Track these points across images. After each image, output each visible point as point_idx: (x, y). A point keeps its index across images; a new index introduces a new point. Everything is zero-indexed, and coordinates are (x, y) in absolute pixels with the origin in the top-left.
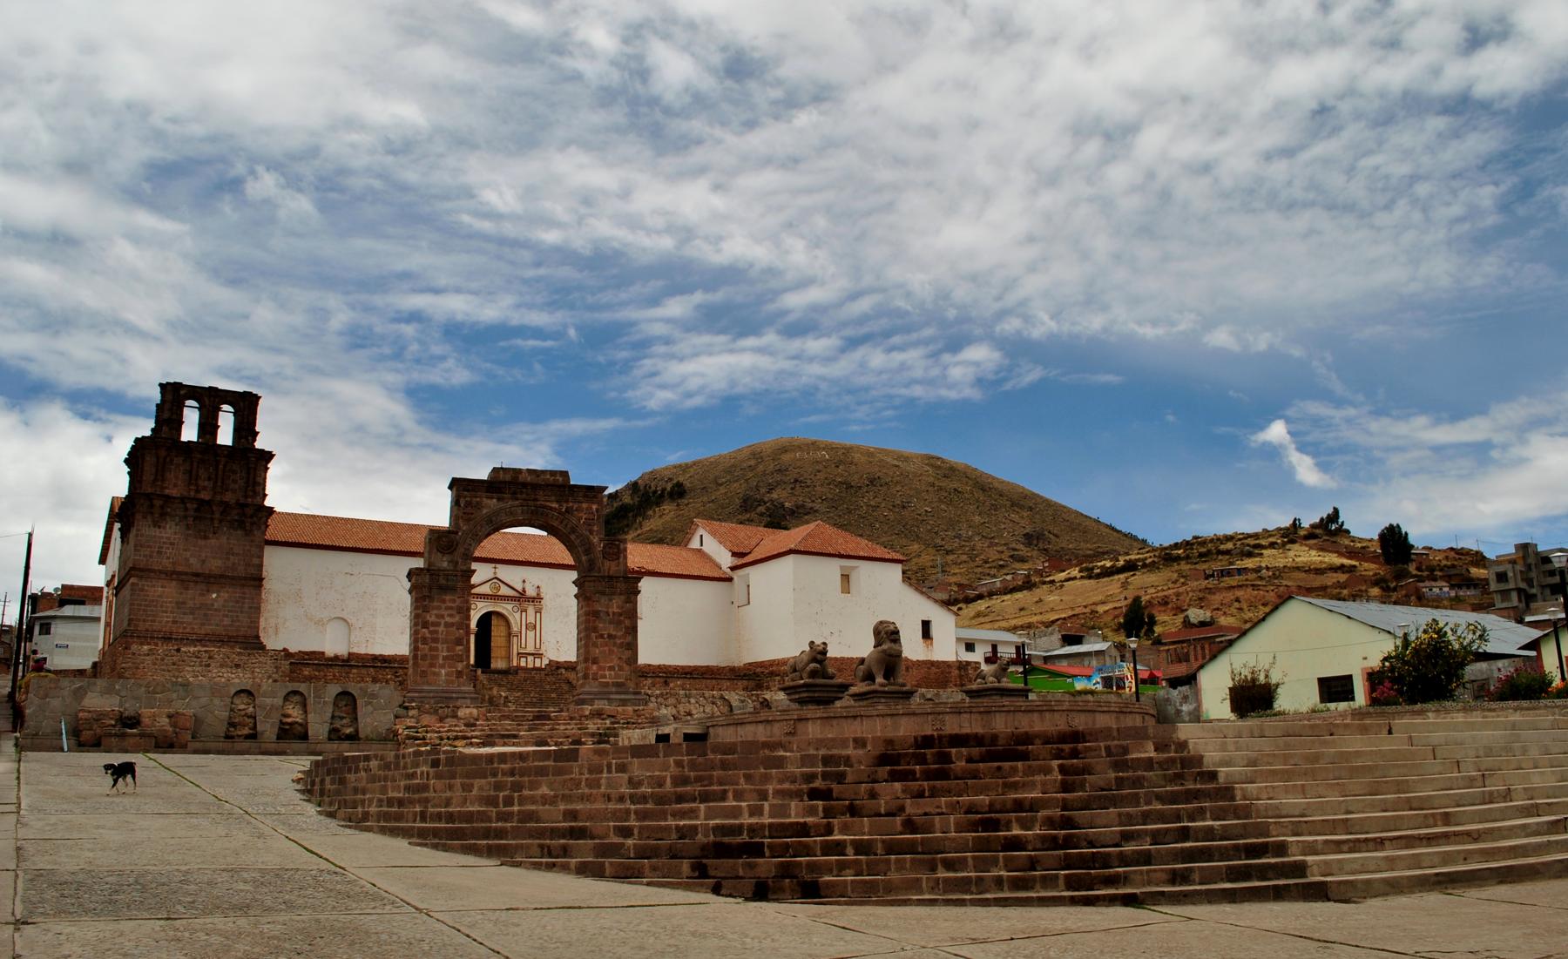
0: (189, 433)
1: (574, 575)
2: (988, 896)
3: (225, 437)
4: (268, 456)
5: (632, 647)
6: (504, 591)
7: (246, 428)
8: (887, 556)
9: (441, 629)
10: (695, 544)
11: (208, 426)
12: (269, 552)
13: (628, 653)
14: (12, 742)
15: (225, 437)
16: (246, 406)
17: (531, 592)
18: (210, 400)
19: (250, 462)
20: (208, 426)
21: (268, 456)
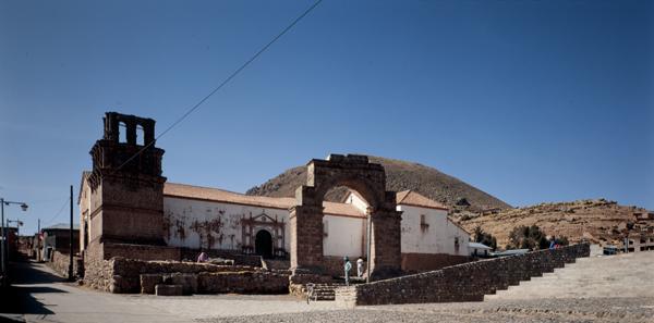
0: (123, 139)
1: (325, 211)
2: (227, 273)
3: (140, 141)
4: (162, 152)
5: (399, 246)
6: (268, 220)
7: (149, 136)
8: (429, 205)
9: (309, 237)
10: (348, 201)
11: (131, 135)
12: (165, 199)
13: (396, 249)
14: (186, 240)
15: (140, 141)
16: (149, 125)
17: (279, 221)
18: (132, 122)
19: (152, 156)
20: (131, 135)
21: (162, 152)
